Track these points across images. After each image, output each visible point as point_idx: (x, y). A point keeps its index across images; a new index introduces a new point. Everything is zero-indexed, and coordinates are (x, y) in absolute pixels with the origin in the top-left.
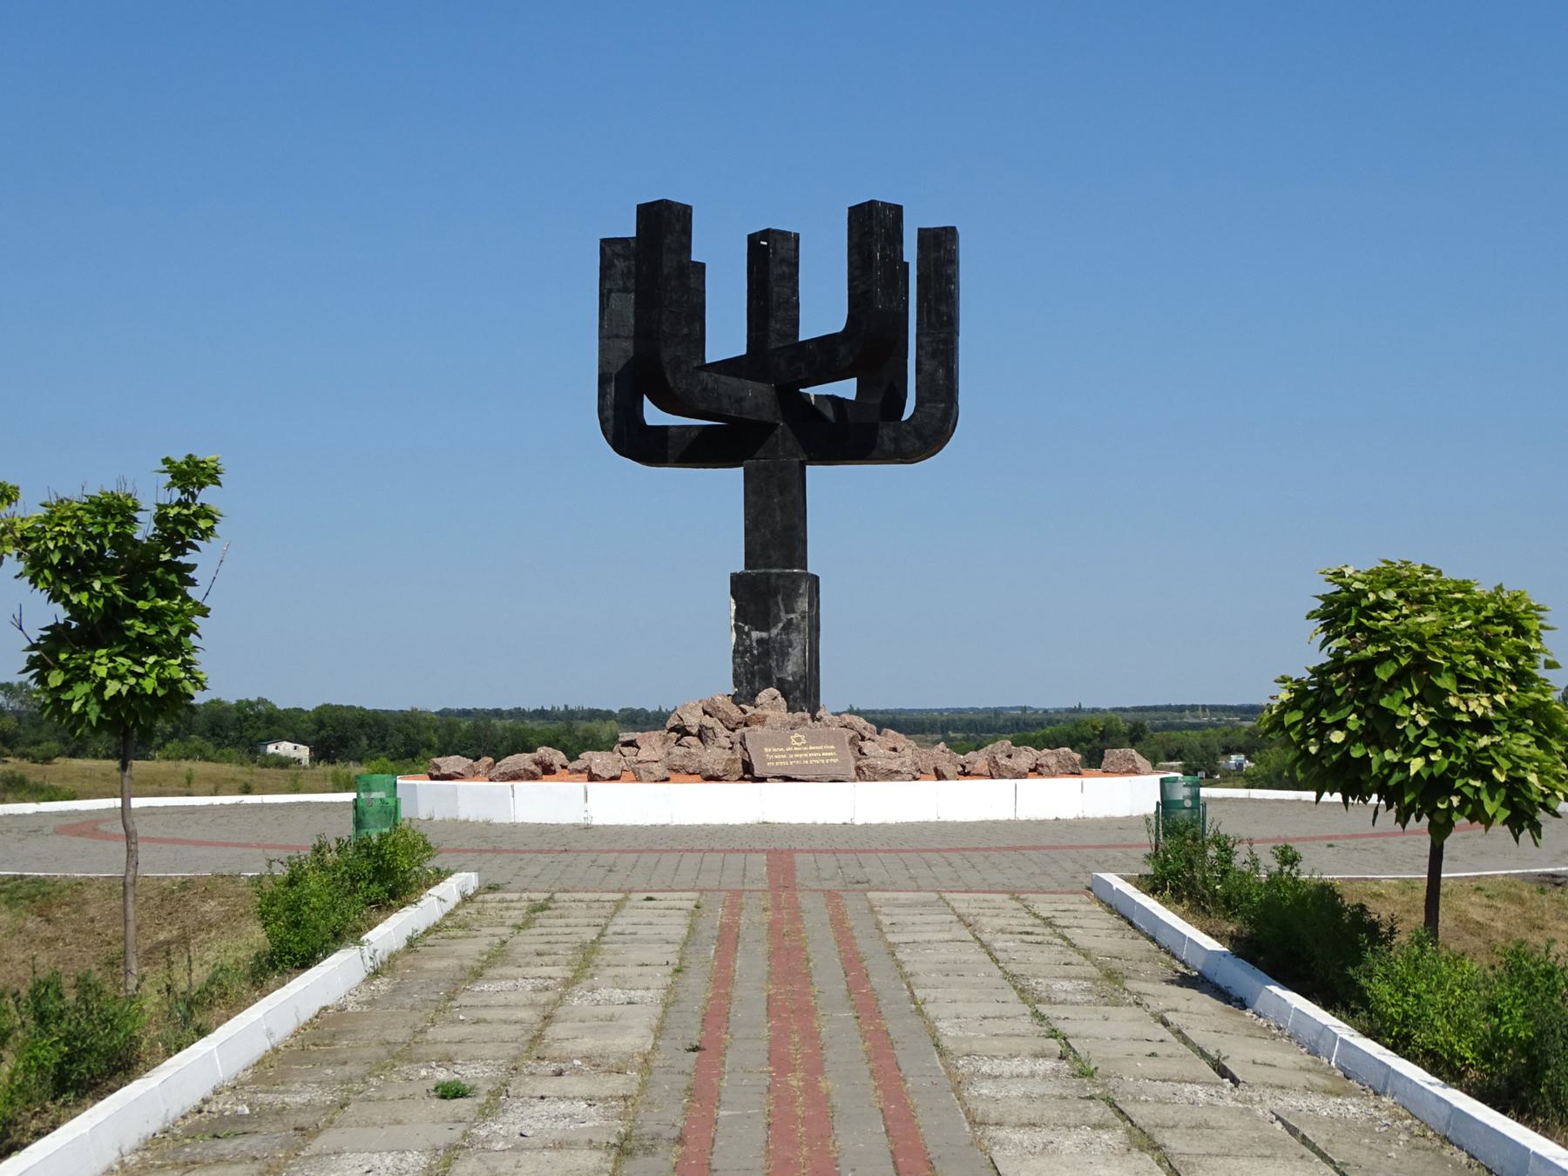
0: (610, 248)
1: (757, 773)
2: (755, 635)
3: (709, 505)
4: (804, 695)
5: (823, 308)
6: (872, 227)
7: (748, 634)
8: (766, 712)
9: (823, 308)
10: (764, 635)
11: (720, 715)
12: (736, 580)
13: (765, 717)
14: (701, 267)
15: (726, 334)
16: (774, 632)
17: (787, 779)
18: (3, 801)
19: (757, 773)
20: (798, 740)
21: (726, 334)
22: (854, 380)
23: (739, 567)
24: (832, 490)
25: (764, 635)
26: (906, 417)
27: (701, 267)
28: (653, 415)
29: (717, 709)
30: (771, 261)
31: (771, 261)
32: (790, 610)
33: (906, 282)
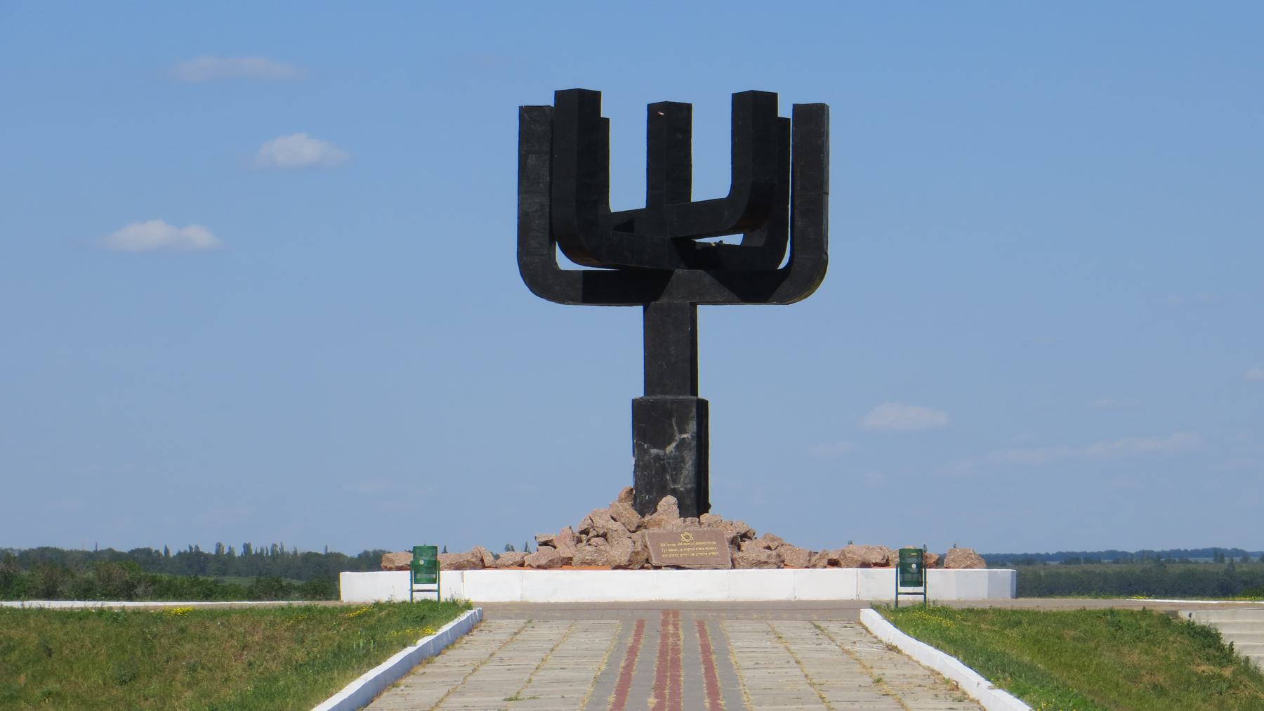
0: (529, 116)
1: (654, 562)
2: (654, 451)
3: (627, 322)
4: (696, 502)
5: (712, 176)
6: (753, 110)
7: (646, 452)
8: (662, 517)
9: (712, 176)
10: (661, 452)
11: (622, 520)
12: (637, 405)
13: (661, 521)
14: (560, 95)
15: (627, 189)
16: (671, 448)
17: (678, 567)
18: (1, 600)
19: (654, 562)
20: (687, 537)
21: (627, 189)
22: (694, 199)
23: (639, 393)
24: (723, 329)
25: (661, 452)
26: (781, 266)
27: (560, 95)
28: (563, 262)
29: (620, 515)
30: (669, 128)
31: (669, 128)
32: (682, 431)
33: (783, 148)
